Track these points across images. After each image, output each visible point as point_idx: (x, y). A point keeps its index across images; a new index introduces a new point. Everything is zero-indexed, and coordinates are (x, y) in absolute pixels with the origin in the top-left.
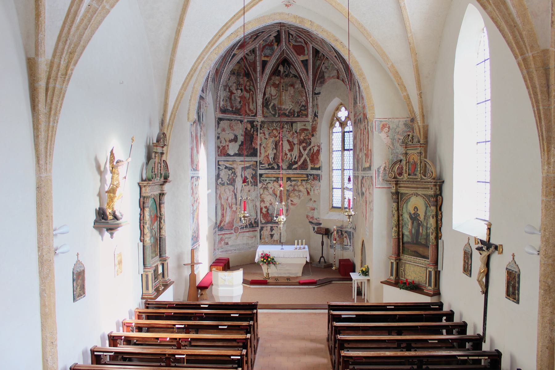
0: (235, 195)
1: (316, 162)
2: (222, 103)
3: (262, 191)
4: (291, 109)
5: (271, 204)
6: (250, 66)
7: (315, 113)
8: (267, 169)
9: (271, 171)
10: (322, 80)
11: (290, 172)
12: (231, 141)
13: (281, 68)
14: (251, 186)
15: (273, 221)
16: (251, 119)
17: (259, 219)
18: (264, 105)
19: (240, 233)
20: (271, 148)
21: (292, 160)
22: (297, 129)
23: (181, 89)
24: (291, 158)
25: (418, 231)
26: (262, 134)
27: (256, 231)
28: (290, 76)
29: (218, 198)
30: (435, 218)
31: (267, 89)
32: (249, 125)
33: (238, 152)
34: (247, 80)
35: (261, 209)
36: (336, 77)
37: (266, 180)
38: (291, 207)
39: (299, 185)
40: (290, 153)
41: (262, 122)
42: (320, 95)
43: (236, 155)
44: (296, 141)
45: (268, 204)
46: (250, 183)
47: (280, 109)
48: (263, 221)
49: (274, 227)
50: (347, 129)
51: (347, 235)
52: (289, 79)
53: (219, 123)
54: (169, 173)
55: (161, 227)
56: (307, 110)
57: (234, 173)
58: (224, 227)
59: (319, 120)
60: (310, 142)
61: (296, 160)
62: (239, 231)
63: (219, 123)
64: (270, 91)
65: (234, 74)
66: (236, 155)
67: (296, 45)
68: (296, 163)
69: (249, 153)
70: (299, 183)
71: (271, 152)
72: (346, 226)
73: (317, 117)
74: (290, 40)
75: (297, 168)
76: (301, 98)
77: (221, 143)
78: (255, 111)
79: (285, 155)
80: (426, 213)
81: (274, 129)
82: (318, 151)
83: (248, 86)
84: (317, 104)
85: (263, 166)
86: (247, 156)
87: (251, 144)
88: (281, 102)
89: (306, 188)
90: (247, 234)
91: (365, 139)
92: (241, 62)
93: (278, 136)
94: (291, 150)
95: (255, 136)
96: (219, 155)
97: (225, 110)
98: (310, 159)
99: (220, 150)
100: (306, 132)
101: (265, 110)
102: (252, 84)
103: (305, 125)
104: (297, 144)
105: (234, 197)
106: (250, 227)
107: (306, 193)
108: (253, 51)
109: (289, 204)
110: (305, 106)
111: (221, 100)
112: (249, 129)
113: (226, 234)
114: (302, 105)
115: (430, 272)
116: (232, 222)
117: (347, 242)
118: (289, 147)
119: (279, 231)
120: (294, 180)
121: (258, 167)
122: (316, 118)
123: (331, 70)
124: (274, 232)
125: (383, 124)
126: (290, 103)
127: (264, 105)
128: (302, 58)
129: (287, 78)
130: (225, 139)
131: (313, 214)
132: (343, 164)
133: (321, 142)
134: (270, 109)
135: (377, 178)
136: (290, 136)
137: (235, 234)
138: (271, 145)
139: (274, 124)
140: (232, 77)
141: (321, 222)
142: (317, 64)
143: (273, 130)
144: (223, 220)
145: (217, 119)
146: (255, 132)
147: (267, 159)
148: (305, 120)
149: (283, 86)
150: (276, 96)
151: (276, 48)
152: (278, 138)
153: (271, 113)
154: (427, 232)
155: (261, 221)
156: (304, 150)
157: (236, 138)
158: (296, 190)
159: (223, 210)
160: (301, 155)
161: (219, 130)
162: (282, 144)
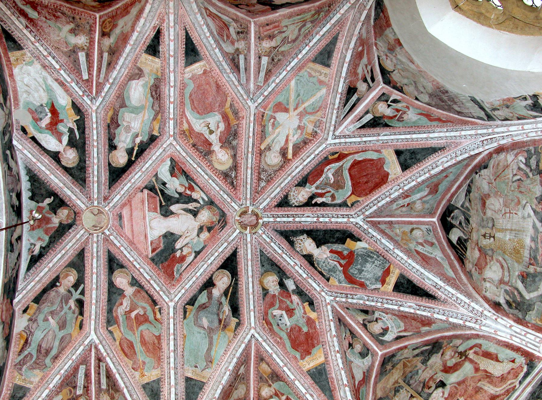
4: (534, 211)
31: (488, 295)
151: (366, 246)
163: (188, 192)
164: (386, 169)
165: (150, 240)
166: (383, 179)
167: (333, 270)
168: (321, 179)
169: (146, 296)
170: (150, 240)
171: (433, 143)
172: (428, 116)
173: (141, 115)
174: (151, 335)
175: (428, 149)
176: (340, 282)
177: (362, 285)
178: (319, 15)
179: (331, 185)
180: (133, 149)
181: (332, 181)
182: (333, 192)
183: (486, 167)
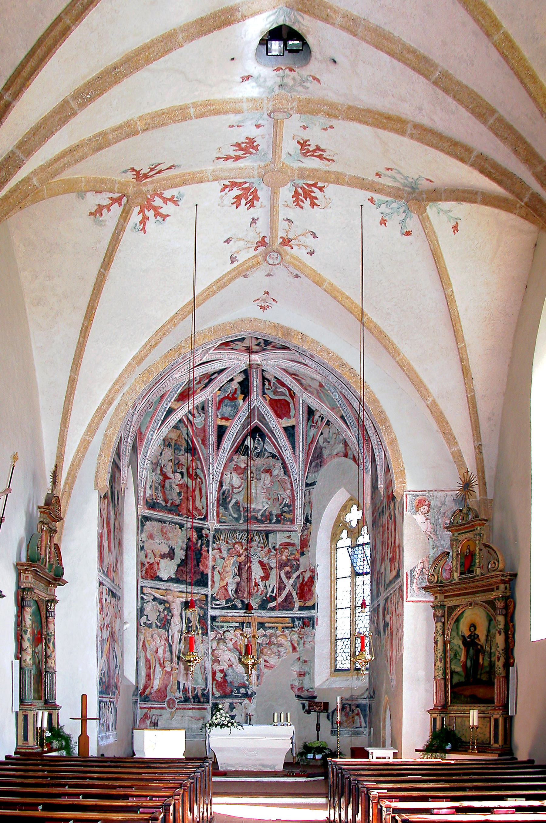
0: (170, 646)
2: (149, 492)
3: (215, 644)
5: (230, 666)
7: (307, 516)
8: (224, 608)
10: (319, 461)
11: (264, 613)
12: (163, 556)
13: (249, 442)
15: (233, 693)
16: (197, 523)
17: (210, 690)
18: (221, 502)
19: (177, 709)
21: (266, 594)
23: (86, 434)
24: (265, 591)
25: (475, 662)
26: (216, 551)
27: (205, 709)
28: (264, 454)
29: (140, 647)
30: (503, 634)
31: (225, 476)
32: (194, 534)
33: (176, 575)
35: (214, 674)
36: (342, 454)
37: (222, 627)
38: (264, 670)
39: (278, 635)
41: (216, 531)
43: (170, 580)
44: (273, 563)
45: (225, 666)
47: (247, 510)
48: (217, 694)
51: (360, 711)
52: (262, 459)
53: (143, 525)
54: (63, 568)
55: (49, 654)
56: (292, 511)
57: (169, 609)
58: (150, 696)
59: (313, 527)
60: (299, 565)
61: (274, 595)
62: (177, 706)
63: (143, 525)
64: (231, 479)
65: (169, 445)
66: (170, 580)
68: (274, 599)
69: (195, 579)
70: (279, 632)
71: (231, 580)
72: (358, 696)
73: (311, 523)
74: (266, 391)
76: (283, 492)
77: (146, 557)
78: (204, 511)
80: (489, 631)
81: (237, 543)
82: (312, 580)
84: (309, 502)
85: (218, 602)
86: (191, 584)
87: (198, 565)
88: (249, 498)
90: (190, 712)
91: (390, 536)
92: (182, 427)
94: (266, 577)
95: (204, 553)
96: (142, 577)
97: (154, 503)
99: (144, 569)
100: (290, 548)
101: (222, 510)
103: (289, 537)
104: (276, 567)
105: (167, 649)
106: (194, 702)
107: (291, 649)
108: (203, 408)
110: (290, 505)
111: (148, 487)
112: (194, 540)
113: (154, 708)
115: (496, 721)
117: (361, 722)
118: (261, 573)
119: (244, 710)
120: (270, 628)
121: (209, 604)
123: (335, 443)
124: (235, 712)
125: (419, 500)
126: (264, 500)
128: (286, 422)
129: (259, 458)
130: (152, 551)
133: (317, 563)
135: (409, 586)
136: (263, 554)
137: (170, 710)
138: (232, 569)
139: (237, 535)
140: (167, 450)
141: (316, 694)
143: (234, 545)
145: (140, 518)
146: (203, 546)
147: (224, 591)
148: (289, 529)
149: (252, 472)
151: (241, 405)
152: (243, 557)
153: (232, 517)
154: (491, 661)
155: (213, 694)
156: (287, 577)
157: (172, 551)
159: (150, 668)
160: (281, 588)
161: (144, 536)
162: (250, 567)
166: (279, 416)
167: (225, 391)
171: (297, 446)
172: (312, 442)
177: (218, 408)
183: (285, 473)
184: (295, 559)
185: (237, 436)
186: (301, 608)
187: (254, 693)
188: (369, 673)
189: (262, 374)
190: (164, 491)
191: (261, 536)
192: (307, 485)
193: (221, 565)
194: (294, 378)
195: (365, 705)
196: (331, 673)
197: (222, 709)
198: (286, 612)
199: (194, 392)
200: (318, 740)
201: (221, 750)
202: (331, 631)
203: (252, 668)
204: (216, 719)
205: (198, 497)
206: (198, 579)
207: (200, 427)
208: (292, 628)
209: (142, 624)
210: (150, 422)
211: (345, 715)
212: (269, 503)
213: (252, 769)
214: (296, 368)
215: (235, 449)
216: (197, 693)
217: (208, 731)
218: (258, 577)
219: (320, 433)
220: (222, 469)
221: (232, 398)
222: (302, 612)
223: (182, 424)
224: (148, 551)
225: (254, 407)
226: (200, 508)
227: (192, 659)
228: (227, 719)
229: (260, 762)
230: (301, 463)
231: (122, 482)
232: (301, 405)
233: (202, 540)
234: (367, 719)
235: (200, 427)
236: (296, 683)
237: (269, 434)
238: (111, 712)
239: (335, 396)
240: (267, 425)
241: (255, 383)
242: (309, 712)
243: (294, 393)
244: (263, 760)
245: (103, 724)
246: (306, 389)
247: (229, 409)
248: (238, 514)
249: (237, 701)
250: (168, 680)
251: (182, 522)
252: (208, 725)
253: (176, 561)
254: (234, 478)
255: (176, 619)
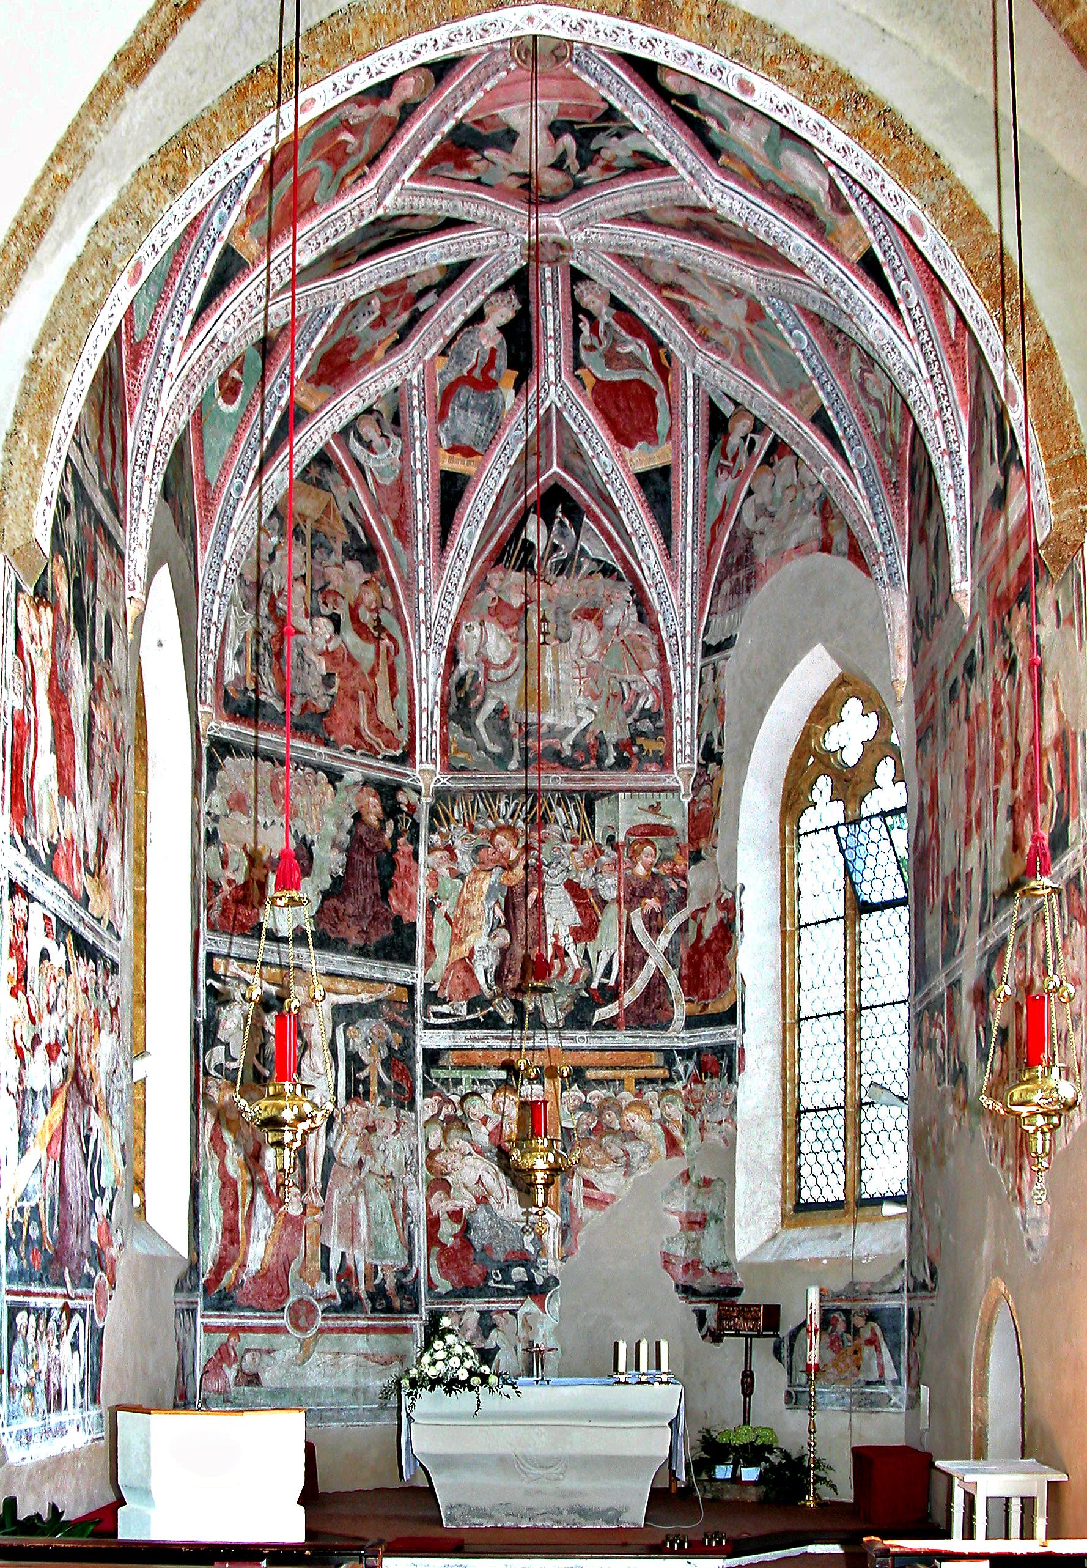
1: (713, 985)
3: (435, 1137)
4: (585, 729)
5: (483, 1200)
6: (377, 510)
8: (462, 1025)
9: (487, 1039)
10: (742, 574)
11: (582, 1039)
13: (534, 531)
14: (383, 1104)
15: (491, 1283)
18: (452, 710)
19: (321, 1331)
20: (482, 921)
21: (589, 980)
22: (615, 828)
24: (585, 971)
26: (438, 854)
27: (406, 1330)
28: (579, 567)
29: (205, 1140)
31: (464, 633)
34: (367, 576)
35: (433, 1224)
36: (815, 545)
37: (457, 1082)
38: (584, 1212)
39: (624, 1104)
40: (581, 945)
41: (441, 795)
42: (731, 652)
45: (465, 1201)
46: (374, 1088)
48: (444, 1286)
49: (499, 1312)
50: (873, 803)
51: (878, 1330)
53: (214, 768)
56: (664, 731)
58: (237, 1293)
59: (728, 775)
60: (684, 891)
61: (612, 982)
62: (319, 1322)
63: (214, 768)
64: (483, 642)
67: (613, 383)
68: (610, 994)
69: (374, 939)
70: (627, 1097)
71: (484, 940)
73: (720, 763)
74: (583, 355)
75: (614, 1019)
76: (635, 676)
77: (225, 864)
78: (403, 736)
79: (555, 956)
81: (500, 829)
83: (371, 611)
84: (715, 701)
85: (444, 1009)
86: (363, 952)
87: (385, 897)
89: (663, 1122)
90: (360, 1343)
92: (336, 484)
93: (522, 863)
94: (586, 932)
95: (403, 861)
96: (211, 926)
98: (680, 978)
99: (218, 899)
100: (660, 841)
101: (456, 733)
102: (389, 603)
103: (654, 809)
104: (618, 900)
106: (374, 1310)
107: (663, 1149)
109: (574, 1198)
111: (230, 652)
112: (373, 820)
114: (643, 709)
116: (281, 1271)
117: (881, 1367)
118: (572, 917)
120: (600, 1082)
122: (713, 767)
123: (791, 516)
124: (495, 1338)
126: (581, 700)
127: (452, 710)
129: (563, 577)
131: (697, 1248)
132: (853, 983)
133: (740, 879)
134: (482, 731)
139: (502, 805)
141: (739, 1280)
142: (719, 495)
143: (493, 834)
144: (234, 1260)
145: (205, 744)
146: (401, 840)
147: (462, 974)
148: (657, 785)
149: (543, 620)
150: (511, 670)
151: (508, 406)
153: (487, 752)
156: (650, 930)
158: (613, 1132)
159: (235, 1207)
160: (634, 960)
162: (539, 901)
163: (601, 163)
164: (639, 444)
165: (500, 111)
166: (624, 438)
167: (461, 358)
168: (624, 333)
169: (385, 139)
170: (500, 111)
172: (721, 519)
173: (763, 153)
174: (312, 189)
175: (670, 527)
176: (441, 376)
177: (442, 416)
178: (890, 454)
179: (612, 348)
180: (694, 106)
181: (619, 349)
182: (601, 348)
183: (641, 618)
184: (674, 875)
185: (499, 513)
186: (692, 1022)
187: (552, 1281)
188: (911, 1213)
189: (573, 291)
190: (281, 669)
191: (571, 806)
192: (708, 650)
193: (453, 899)
194: (669, 302)
195: (897, 1312)
196: (783, 1216)
197: (450, 1331)
198: (647, 1033)
199: (368, 356)
200: (746, 1421)
201: (448, 1462)
202: (784, 1088)
203: (547, 1185)
204: (433, 1363)
205: (384, 694)
206: (384, 940)
207: (388, 483)
208: (665, 1081)
209: (212, 1072)
210: (234, 448)
211: (832, 1343)
212: (595, 709)
213: (548, 1524)
214: (678, 252)
215: (492, 552)
216: (384, 1280)
217: (406, 1401)
218: (564, 931)
219: (743, 494)
220: (455, 608)
221: (485, 384)
222: (697, 1032)
223: (337, 476)
224: (231, 847)
225: (549, 409)
226: (391, 724)
227: (288, 1115)
228: (468, 1364)
229: (574, 1501)
230: (689, 582)
231: (129, 594)
232: (690, 392)
233: (396, 822)
234: (903, 1357)
235: (388, 483)
236: (680, 1250)
237: (594, 506)
238: (75, 1346)
239: (798, 340)
240: (586, 476)
241: (550, 325)
242: (716, 1337)
243: (669, 356)
244: (580, 1493)
245: (30, 1389)
246: (704, 338)
247: (474, 418)
248: (504, 745)
249: (504, 1306)
250: (293, 1242)
251: (336, 764)
252: (405, 1383)
253: (316, 881)
254: (492, 638)
255: (315, 1058)
